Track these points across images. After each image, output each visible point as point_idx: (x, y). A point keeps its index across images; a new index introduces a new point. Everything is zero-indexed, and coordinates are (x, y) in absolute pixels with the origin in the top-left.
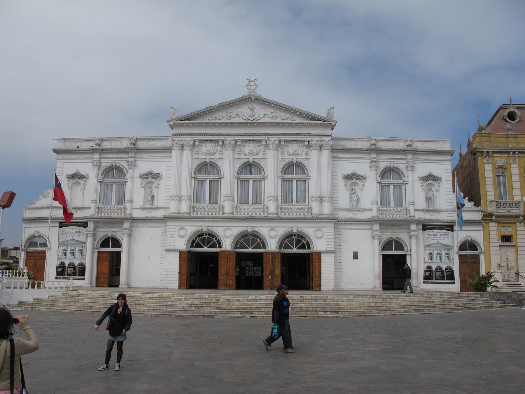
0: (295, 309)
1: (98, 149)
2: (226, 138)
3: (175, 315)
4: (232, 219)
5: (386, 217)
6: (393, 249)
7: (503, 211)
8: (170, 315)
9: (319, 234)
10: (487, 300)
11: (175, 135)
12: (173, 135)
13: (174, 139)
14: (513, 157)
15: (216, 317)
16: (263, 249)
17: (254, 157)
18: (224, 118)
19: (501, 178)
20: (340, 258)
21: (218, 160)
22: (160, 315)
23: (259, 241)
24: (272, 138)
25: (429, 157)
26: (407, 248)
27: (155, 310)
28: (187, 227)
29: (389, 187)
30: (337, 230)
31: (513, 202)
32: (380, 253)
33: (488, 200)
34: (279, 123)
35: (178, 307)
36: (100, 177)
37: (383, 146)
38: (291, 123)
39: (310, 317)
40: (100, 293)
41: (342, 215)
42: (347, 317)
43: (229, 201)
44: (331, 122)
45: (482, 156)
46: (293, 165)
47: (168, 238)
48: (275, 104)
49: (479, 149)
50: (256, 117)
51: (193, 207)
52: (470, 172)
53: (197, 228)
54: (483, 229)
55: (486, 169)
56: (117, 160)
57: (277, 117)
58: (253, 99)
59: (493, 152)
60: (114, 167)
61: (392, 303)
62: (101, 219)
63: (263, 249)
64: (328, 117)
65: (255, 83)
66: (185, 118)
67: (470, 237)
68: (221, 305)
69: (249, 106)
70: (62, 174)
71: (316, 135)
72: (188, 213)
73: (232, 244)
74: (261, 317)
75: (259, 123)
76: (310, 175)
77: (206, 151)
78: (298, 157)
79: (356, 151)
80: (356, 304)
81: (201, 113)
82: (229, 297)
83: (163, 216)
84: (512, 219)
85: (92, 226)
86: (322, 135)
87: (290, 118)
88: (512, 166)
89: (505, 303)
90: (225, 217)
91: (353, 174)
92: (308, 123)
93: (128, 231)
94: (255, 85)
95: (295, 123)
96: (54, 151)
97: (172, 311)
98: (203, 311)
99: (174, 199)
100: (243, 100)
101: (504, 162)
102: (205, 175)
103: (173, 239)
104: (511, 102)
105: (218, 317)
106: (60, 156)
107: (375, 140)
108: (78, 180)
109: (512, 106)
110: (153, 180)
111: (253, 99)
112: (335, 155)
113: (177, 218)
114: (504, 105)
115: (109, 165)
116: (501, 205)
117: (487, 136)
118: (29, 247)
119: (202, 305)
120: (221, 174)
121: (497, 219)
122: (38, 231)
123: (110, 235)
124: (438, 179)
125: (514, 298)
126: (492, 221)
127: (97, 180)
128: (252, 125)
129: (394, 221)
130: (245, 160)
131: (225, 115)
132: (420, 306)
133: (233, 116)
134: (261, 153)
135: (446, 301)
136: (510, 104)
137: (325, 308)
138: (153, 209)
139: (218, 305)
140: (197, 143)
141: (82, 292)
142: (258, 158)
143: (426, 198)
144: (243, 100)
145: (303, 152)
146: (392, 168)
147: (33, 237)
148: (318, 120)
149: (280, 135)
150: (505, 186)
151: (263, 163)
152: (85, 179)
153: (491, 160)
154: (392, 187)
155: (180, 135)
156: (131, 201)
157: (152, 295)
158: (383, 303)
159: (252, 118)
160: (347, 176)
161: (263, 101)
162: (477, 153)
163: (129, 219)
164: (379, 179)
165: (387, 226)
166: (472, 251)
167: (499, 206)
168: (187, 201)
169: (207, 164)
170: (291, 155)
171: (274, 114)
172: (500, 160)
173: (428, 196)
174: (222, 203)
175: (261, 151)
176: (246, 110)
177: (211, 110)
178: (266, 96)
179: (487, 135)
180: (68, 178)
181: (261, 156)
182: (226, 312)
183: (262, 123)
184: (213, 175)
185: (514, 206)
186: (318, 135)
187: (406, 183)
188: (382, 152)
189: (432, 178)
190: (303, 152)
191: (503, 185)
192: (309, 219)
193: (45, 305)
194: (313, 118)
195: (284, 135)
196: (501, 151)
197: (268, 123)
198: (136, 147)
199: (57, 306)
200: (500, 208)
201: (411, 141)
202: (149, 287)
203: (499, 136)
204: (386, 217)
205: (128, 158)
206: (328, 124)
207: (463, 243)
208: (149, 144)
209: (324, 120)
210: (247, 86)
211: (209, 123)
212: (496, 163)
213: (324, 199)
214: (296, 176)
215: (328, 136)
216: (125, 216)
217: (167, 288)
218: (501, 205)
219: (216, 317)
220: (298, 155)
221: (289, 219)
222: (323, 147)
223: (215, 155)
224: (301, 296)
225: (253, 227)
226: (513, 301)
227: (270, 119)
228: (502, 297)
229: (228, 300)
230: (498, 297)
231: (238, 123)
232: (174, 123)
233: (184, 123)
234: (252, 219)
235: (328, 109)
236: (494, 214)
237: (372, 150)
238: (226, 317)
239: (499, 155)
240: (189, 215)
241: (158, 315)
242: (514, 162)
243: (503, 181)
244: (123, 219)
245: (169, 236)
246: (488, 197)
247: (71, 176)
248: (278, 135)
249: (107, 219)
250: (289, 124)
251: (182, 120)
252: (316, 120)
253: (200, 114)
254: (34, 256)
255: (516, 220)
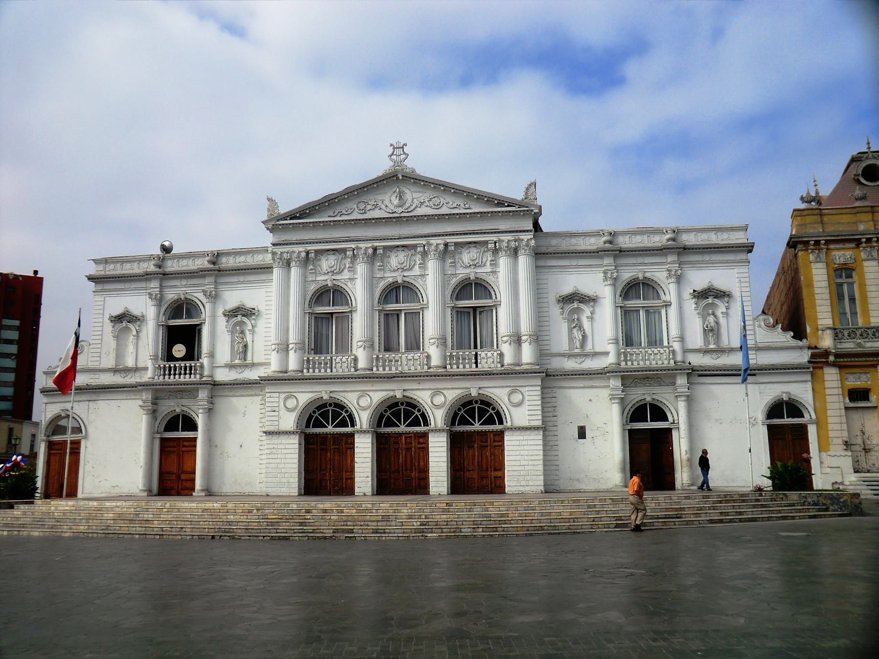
0: (427, 524)
1: (157, 272)
2: (358, 245)
3: (229, 536)
4: (369, 377)
5: (632, 364)
6: (649, 419)
7: (849, 346)
8: (221, 536)
9: (517, 398)
10: (794, 506)
11: (277, 245)
12: (274, 245)
13: (274, 250)
14: (868, 247)
15: (291, 538)
16: (424, 426)
17: (406, 274)
18: (355, 213)
19: (845, 287)
20: (556, 438)
21: (489, 275)
22: (205, 537)
23: (417, 413)
24: (434, 241)
25: (707, 258)
26: (673, 417)
27: (203, 529)
28: (297, 394)
29: (638, 312)
30: (546, 390)
31: (868, 329)
32: (624, 427)
33: (820, 327)
34: (443, 215)
35: (241, 524)
36: (162, 318)
37: (625, 244)
38: (464, 214)
39: (444, 537)
40: (134, 504)
41: (697, 360)
42: (507, 536)
43: (510, 344)
44: (532, 209)
45: (807, 250)
46: (472, 283)
47: (268, 414)
48: (436, 184)
49: (802, 237)
50: (407, 205)
51: (308, 360)
52: (792, 278)
53: (314, 394)
54: (812, 379)
55: (814, 272)
56: (189, 290)
57: (440, 206)
58: (401, 178)
59: (826, 241)
60: (183, 300)
61: (602, 512)
62: (163, 385)
63: (424, 426)
64: (527, 201)
65: (403, 151)
66: (291, 215)
67: (788, 394)
68: (310, 519)
69: (394, 190)
70: (103, 315)
71: (506, 232)
72: (299, 371)
73: (371, 420)
74: (363, 538)
75: (411, 216)
76: (498, 299)
77: (469, 261)
78: (478, 270)
79: (578, 254)
80: (536, 514)
81: (316, 205)
82: (330, 505)
83: (259, 377)
84: (868, 359)
85: (150, 398)
86: (517, 231)
87: (462, 205)
88: (866, 264)
89: (829, 511)
90: (360, 375)
91: (573, 294)
92: (492, 212)
93: (205, 403)
94: (404, 153)
95: (471, 213)
96: (89, 279)
97: (228, 530)
98: (275, 529)
99: (294, 348)
100: (383, 180)
101: (851, 257)
102: (397, 305)
103: (276, 414)
104: (869, 148)
105: (293, 538)
106: (100, 287)
107: (674, 231)
108: (128, 323)
109: (871, 155)
110: (245, 319)
111: (401, 178)
112: (542, 263)
113: (281, 379)
114: (859, 155)
115: (176, 297)
116: (858, 334)
117: (816, 213)
118: (54, 434)
119: (281, 519)
120: (352, 304)
121: (838, 360)
122: (66, 408)
123: (178, 410)
124: (724, 295)
125: (844, 501)
126: (828, 364)
127: (158, 323)
128: (398, 220)
129: (646, 371)
130: (391, 280)
131: (355, 206)
132: (651, 517)
133: (369, 207)
134: (417, 267)
135: (708, 508)
136: (866, 153)
137: (477, 522)
138: (246, 366)
139: (305, 519)
140: (312, 255)
141: (109, 504)
142: (483, 272)
143: (705, 330)
144: (383, 180)
145: (486, 261)
146: (642, 280)
147: (58, 417)
148: (508, 206)
149: (446, 235)
150: (852, 300)
151: (493, 279)
152: (138, 323)
153: (823, 255)
154: (642, 313)
155: (284, 244)
156: (212, 355)
157: (211, 505)
158: (586, 513)
159: (400, 210)
160: (563, 298)
161: (416, 179)
162: (797, 246)
163: (207, 384)
164: (619, 300)
165: (636, 380)
166: (793, 418)
167: (840, 336)
168: (298, 351)
169: (399, 285)
170: (466, 267)
171: (436, 201)
172: (841, 255)
173: (707, 327)
174: (354, 352)
175: (418, 263)
176: (390, 197)
177: (332, 199)
178: (423, 170)
179: (817, 211)
180: (112, 321)
181: (417, 271)
182: (311, 531)
183: (415, 216)
184: (340, 307)
185: (871, 335)
186: (510, 232)
187: (667, 305)
188: (222, 272)
189: (713, 294)
190: (486, 261)
191: (849, 299)
192: (497, 374)
193: (41, 526)
194: (500, 203)
195: (453, 235)
196: (844, 238)
197: (425, 216)
198: (616, 247)
199: (58, 526)
200: (842, 341)
201: (674, 231)
202: (242, 494)
203: (840, 211)
204: (632, 364)
205: (203, 286)
206: (526, 212)
207: (772, 407)
208: (237, 261)
209: (520, 205)
210: (391, 156)
211: (330, 221)
212: (835, 261)
213: (524, 338)
214: (477, 301)
215: (528, 231)
216: (202, 379)
217: (268, 495)
218: (844, 336)
219: (291, 538)
220: (478, 266)
221: (464, 375)
222: (519, 251)
223: (343, 273)
224: (447, 503)
225: (404, 390)
226: (843, 506)
227: (430, 208)
228: (821, 500)
229: (325, 511)
230: (815, 499)
231: (377, 219)
232: (273, 225)
233: (290, 224)
234: (402, 377)
235: (526, 186)
236: (830, 352)
237: (605, 251)
238: (307, 538)
239: (838, 246)
240: (301, 374)
241: (203, 537)
242: (870, 257)
243: (848, 291)
244: (197, 384)
245: (269, 409)
246: (820, 322)
247: (116, 317)
248: (443, 235)
249: (172, 385)
250: (461, 216)
251: (286, 220)
252: (506, 206)
253: (305, 211)
254: (61, 450)
255: (872, 361)
